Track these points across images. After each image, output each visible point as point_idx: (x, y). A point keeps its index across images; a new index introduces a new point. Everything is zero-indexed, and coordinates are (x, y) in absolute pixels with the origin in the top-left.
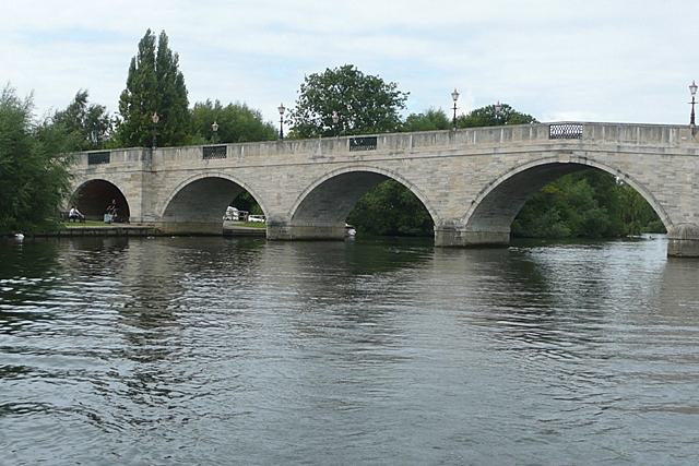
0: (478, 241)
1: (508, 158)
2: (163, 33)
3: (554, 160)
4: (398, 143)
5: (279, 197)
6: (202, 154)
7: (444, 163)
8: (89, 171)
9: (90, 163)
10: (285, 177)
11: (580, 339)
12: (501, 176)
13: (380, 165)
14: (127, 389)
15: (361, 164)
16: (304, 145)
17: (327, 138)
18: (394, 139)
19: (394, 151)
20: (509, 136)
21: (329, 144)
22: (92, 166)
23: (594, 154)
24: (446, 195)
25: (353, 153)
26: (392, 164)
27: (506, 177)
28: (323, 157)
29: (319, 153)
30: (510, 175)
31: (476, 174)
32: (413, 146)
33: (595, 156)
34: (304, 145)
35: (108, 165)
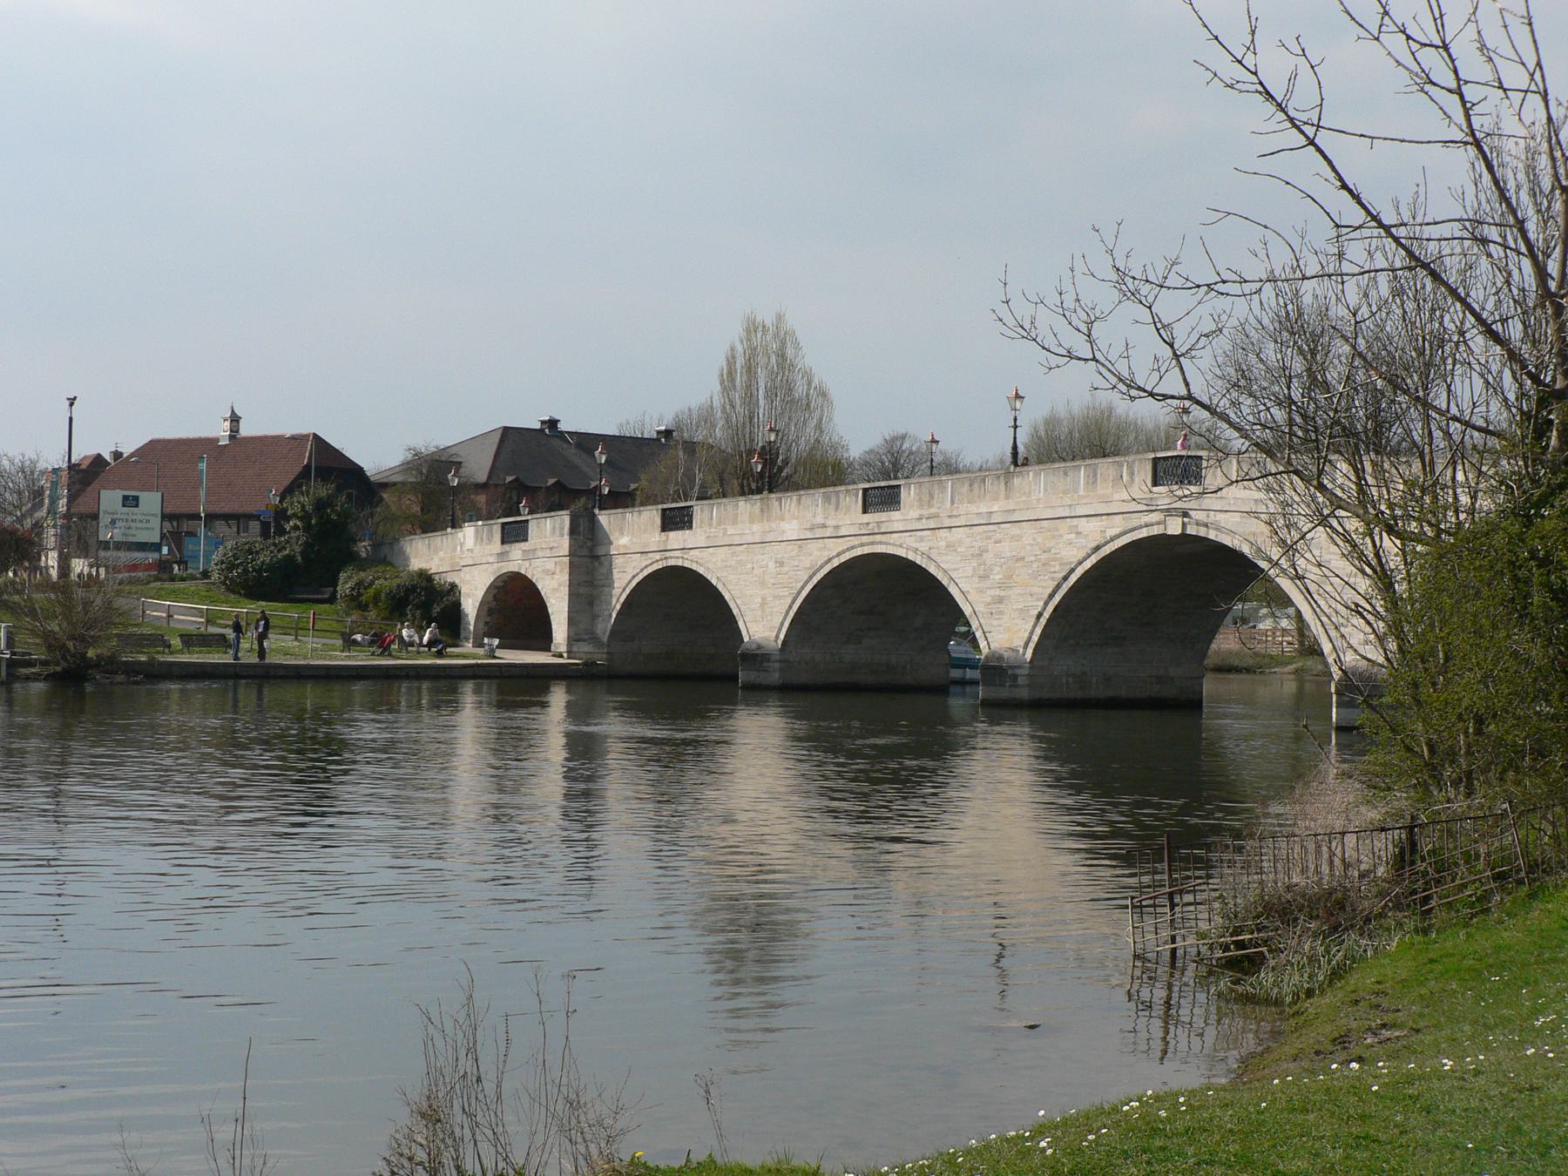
0: (1079, 695)
1: (1095, 524)
2: (780, 318)
3: (1156, 530)
4: (932, 496)
5: (764, 603)
6: (658, 521)
7: (998, 536)
8: (502, 556)
9: (503, 542)
10: (771, 565)
11: (241, 849)
12: (1080, 563)
13: (909, 540)
14: (728, 977)
15: (878, 538)
16: (799, 500)
17: (831, 489)
18: (925, 490)
19: (925, 512)
20: (1093, 480)
21: (834, 500)
22: (507, 547)
23: (1220, 516)
24: (1000, 600)
25: (867, 518)
26: (922, 539)
27: (1088, 564)
28: (824, 526)
29: (819, 520)
30: (1093, 560)
31: (1044, 556)
32: (952, 502)
33: (1221, 518)
34: (799, 500)
35: (524, 546)
